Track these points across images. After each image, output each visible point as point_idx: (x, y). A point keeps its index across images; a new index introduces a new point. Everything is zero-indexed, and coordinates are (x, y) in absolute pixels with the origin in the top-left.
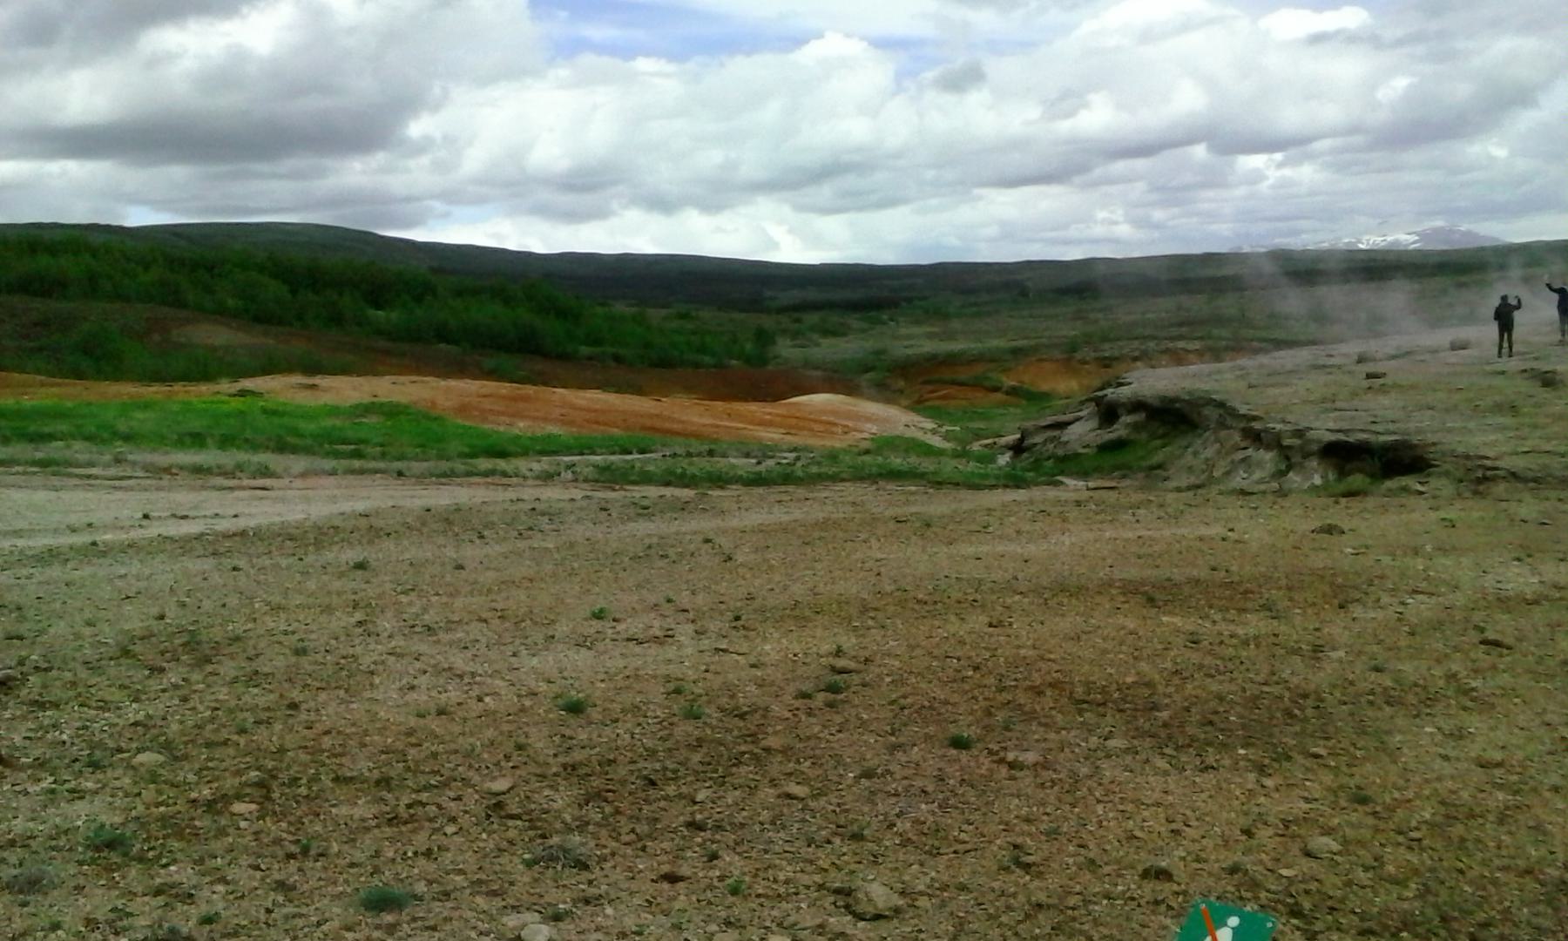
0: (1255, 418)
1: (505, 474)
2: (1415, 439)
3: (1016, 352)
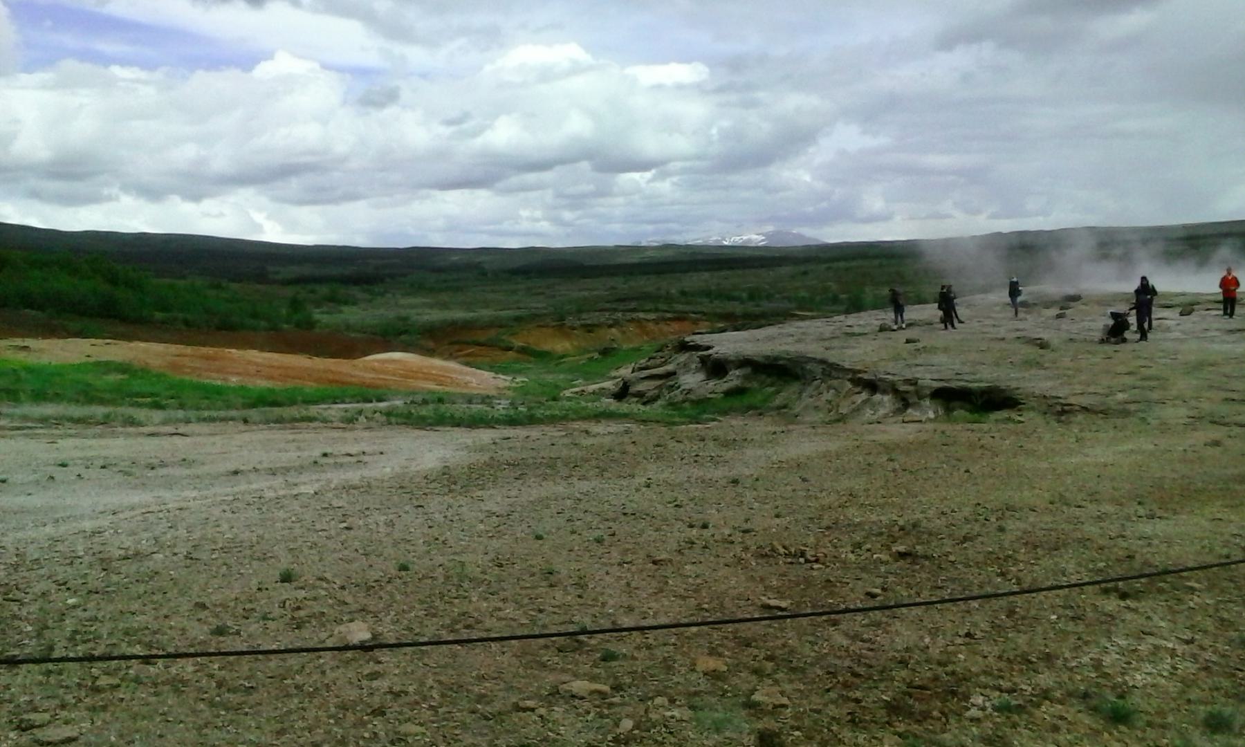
0: (859, 372)
1: (311, 419)
2: (1003, 385)
3: (518, 319)
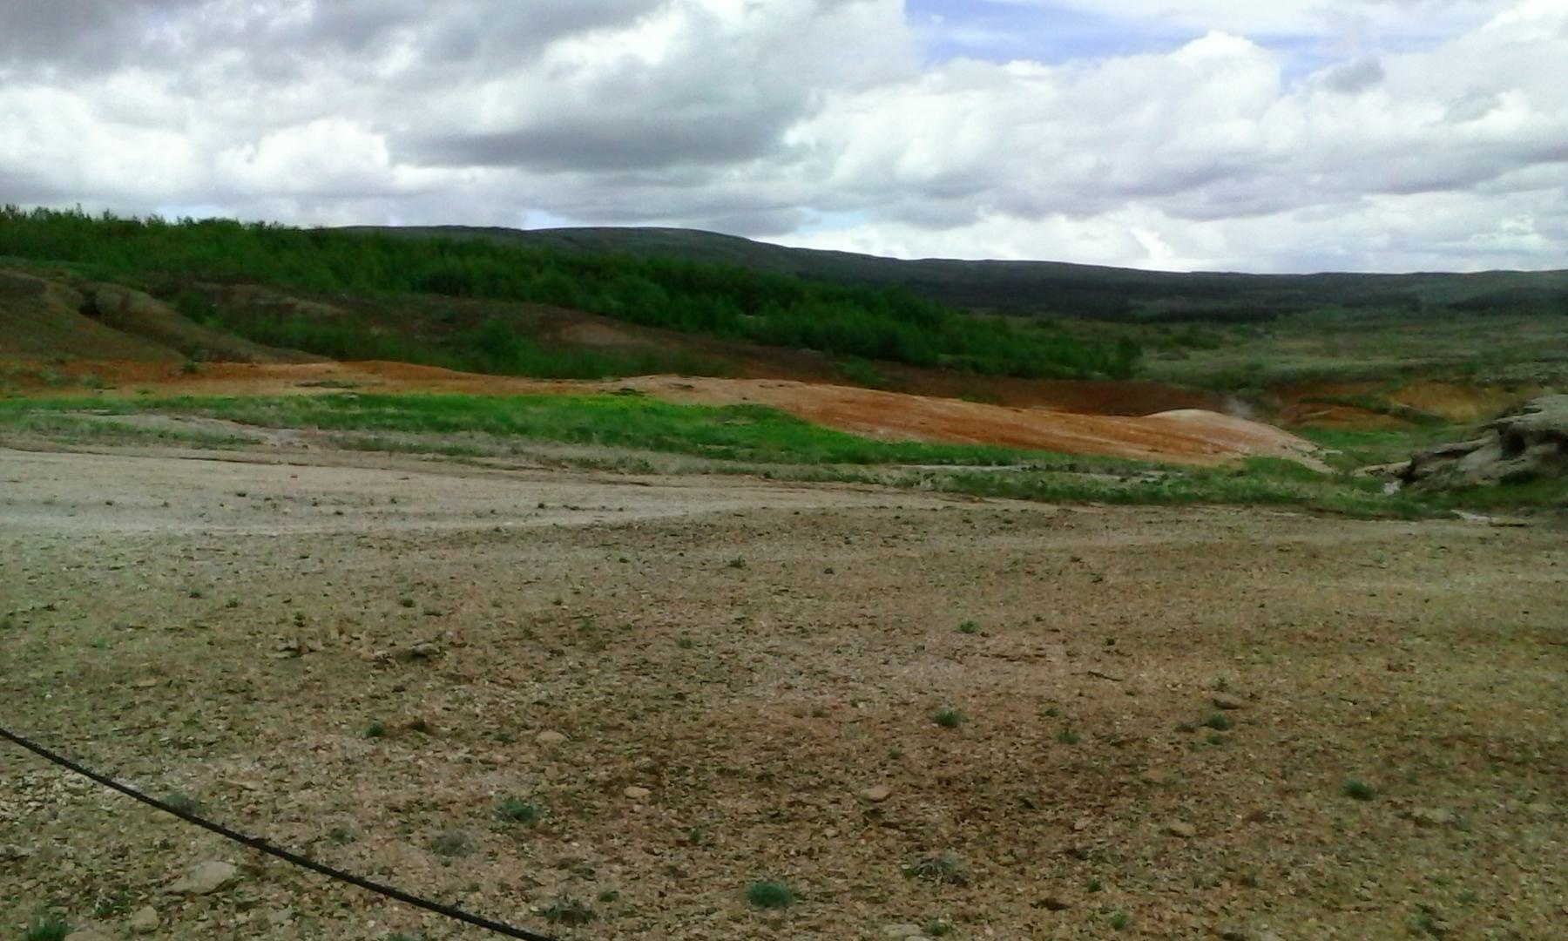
3: (1405, 370)
